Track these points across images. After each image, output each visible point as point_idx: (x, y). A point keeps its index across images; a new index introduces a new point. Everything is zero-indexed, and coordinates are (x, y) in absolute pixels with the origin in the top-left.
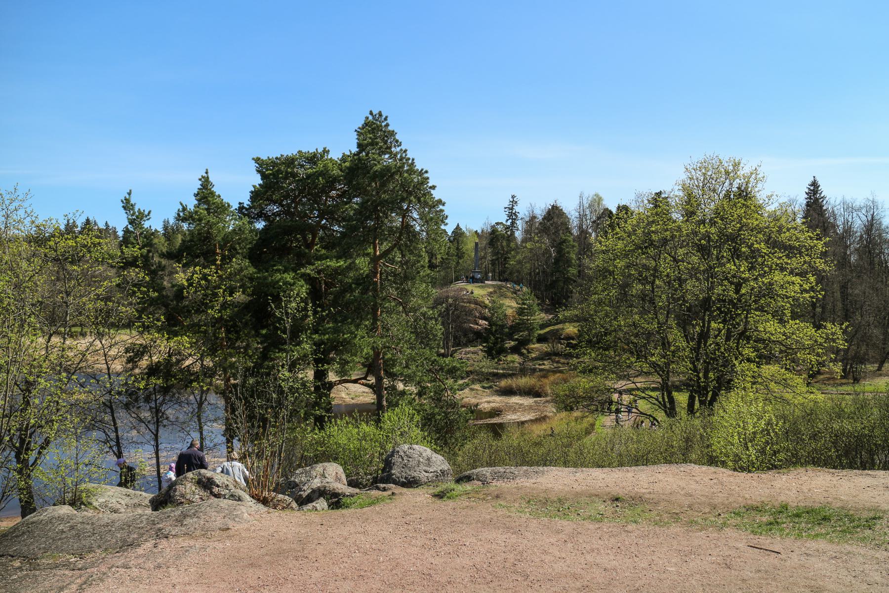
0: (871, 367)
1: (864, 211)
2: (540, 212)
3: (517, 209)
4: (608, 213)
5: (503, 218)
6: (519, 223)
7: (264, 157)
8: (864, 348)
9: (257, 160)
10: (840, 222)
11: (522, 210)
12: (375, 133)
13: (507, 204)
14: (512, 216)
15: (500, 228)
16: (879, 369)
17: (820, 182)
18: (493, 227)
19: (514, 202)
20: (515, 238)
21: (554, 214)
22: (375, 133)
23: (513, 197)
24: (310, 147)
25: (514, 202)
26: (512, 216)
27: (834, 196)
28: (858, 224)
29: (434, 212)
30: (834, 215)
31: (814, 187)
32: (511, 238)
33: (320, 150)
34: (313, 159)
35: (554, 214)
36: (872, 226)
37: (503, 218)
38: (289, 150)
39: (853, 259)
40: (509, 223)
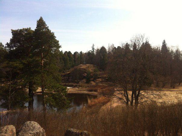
0: (178, 84)
1: (176, 47)
2: (99, 48)
3: (94, 47)
4: (115, 48)
5: (91, 49)
6: (95, 51)
7: (14, 29)
8: (176, 80)
9: (12, 30)
10: (170, 49)
11: (96, 48)
12: (41, 23)
13: (92, 46)
14: (93, 49)
15: (90, 52)
16: (179, 85)
17: (165, 40)
18: (89, 52)
19: (93, 46)
20: (94, 54)
21: (103, 49)
22: (41, 23)
23: (93, 44)
24: (26, 27)
25: (93, 46)
26: (93, 49)
27: (169, 45)
28: (174, 50)
29: (57, 44)
30: (169, 48)
31: (164, 42)
32: (93, 54)
33: (29, 28)
34: (26, 30)
35: (103, 49)
36: (177, 51)
37: (91, 49)
38: (21, 28)
39: (173, 58)
40: (92, 51)
